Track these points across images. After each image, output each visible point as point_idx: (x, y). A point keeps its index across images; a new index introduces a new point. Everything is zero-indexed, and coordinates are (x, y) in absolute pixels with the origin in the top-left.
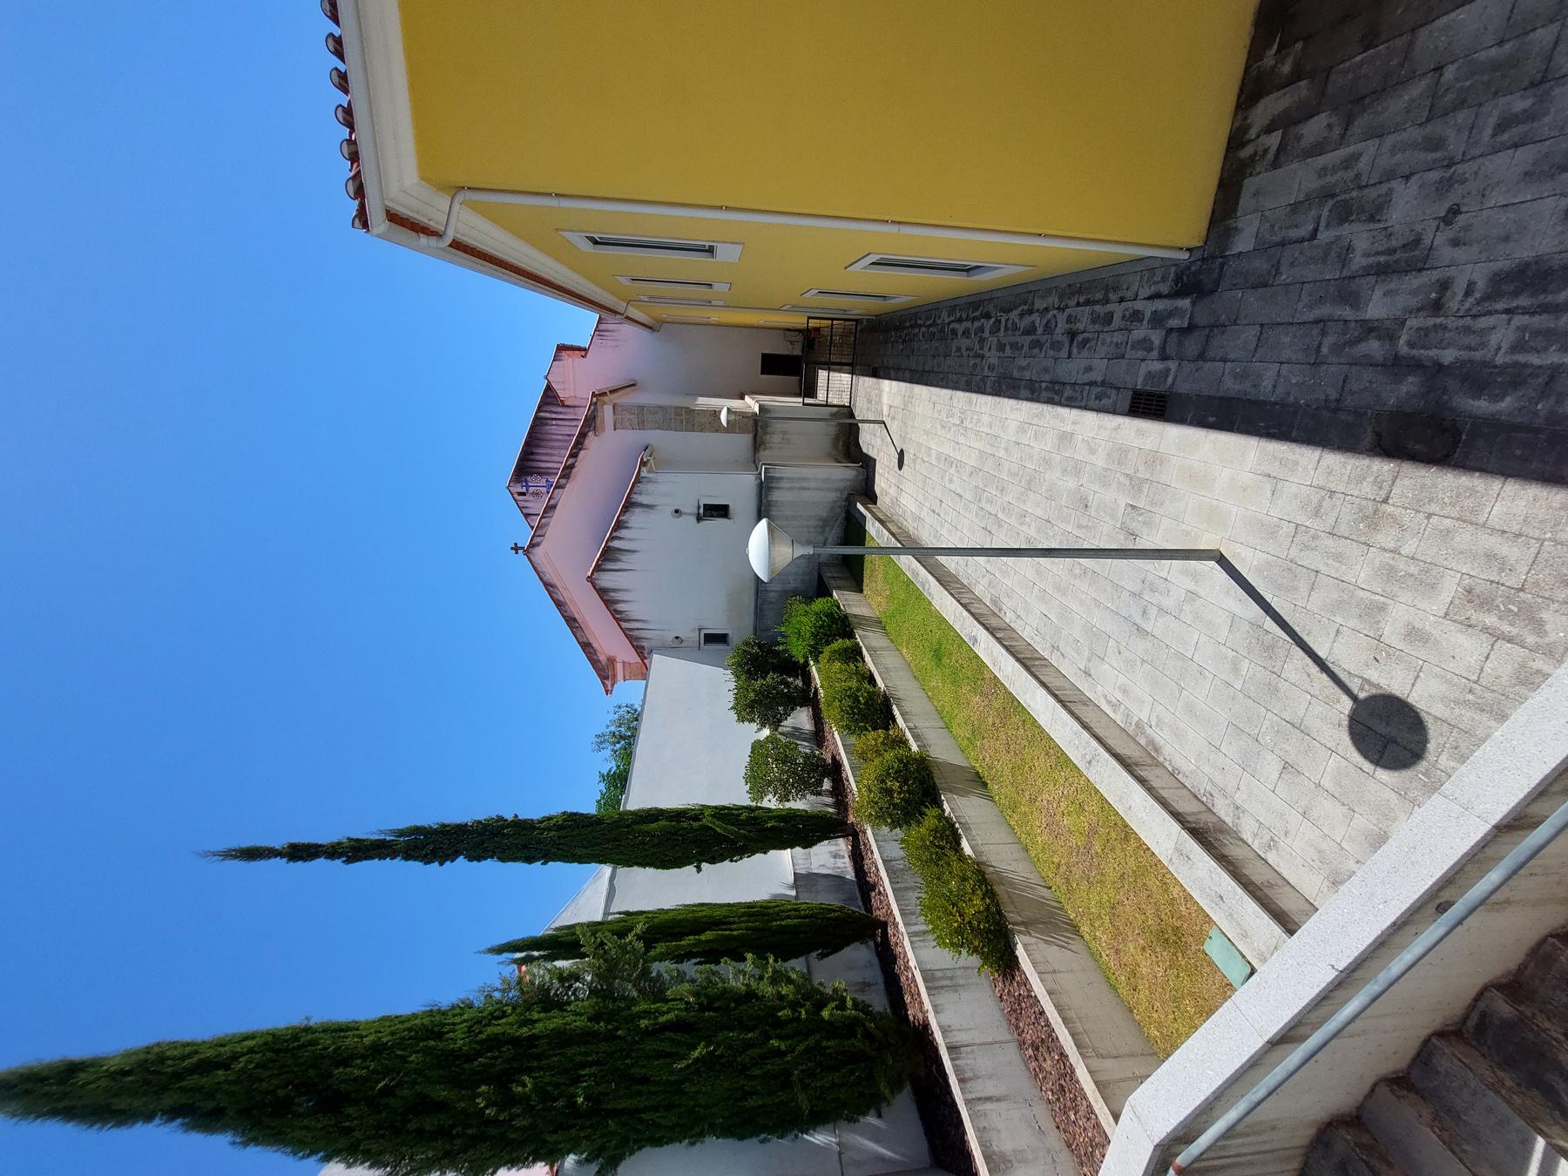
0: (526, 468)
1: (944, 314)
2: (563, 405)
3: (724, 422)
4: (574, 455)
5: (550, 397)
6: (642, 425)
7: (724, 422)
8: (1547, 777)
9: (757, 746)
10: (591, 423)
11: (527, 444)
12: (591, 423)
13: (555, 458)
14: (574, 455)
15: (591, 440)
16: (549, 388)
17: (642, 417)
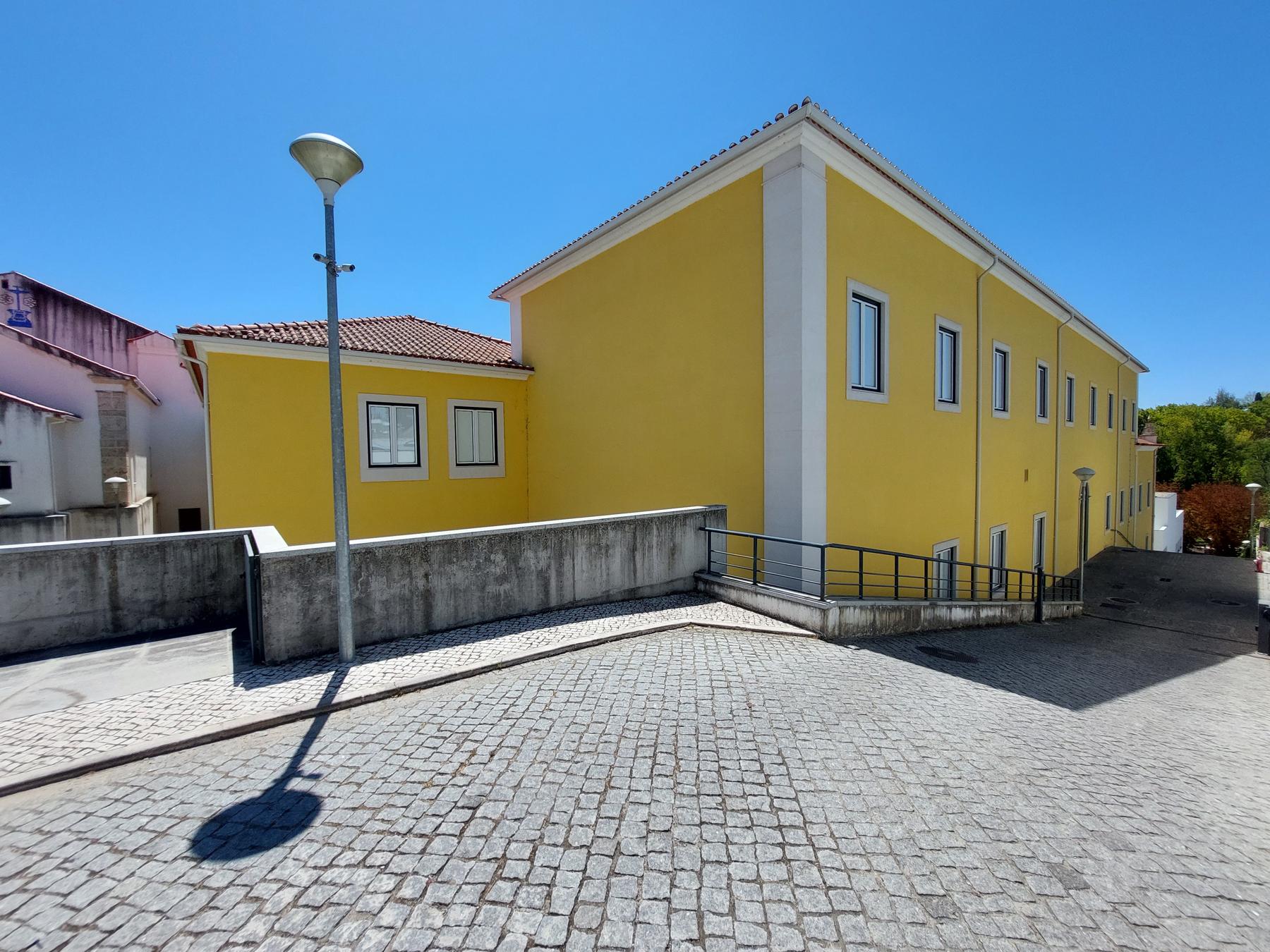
0: (42, 295)
1: (1158, 578)
2: (126, 343)
3: (109, 480)
4: (63, 354)
5: (135, 332)
6: (103, 413)
7: (109, 480)
8: (487, 636)
9: (233, 633)
10: (102, 373)
11: (99, 311)
12: (102, 373)
13: (63, 334)
14: (63, 354)
15: (82, 372)
16: (146, 333)
17: (114, 416)
